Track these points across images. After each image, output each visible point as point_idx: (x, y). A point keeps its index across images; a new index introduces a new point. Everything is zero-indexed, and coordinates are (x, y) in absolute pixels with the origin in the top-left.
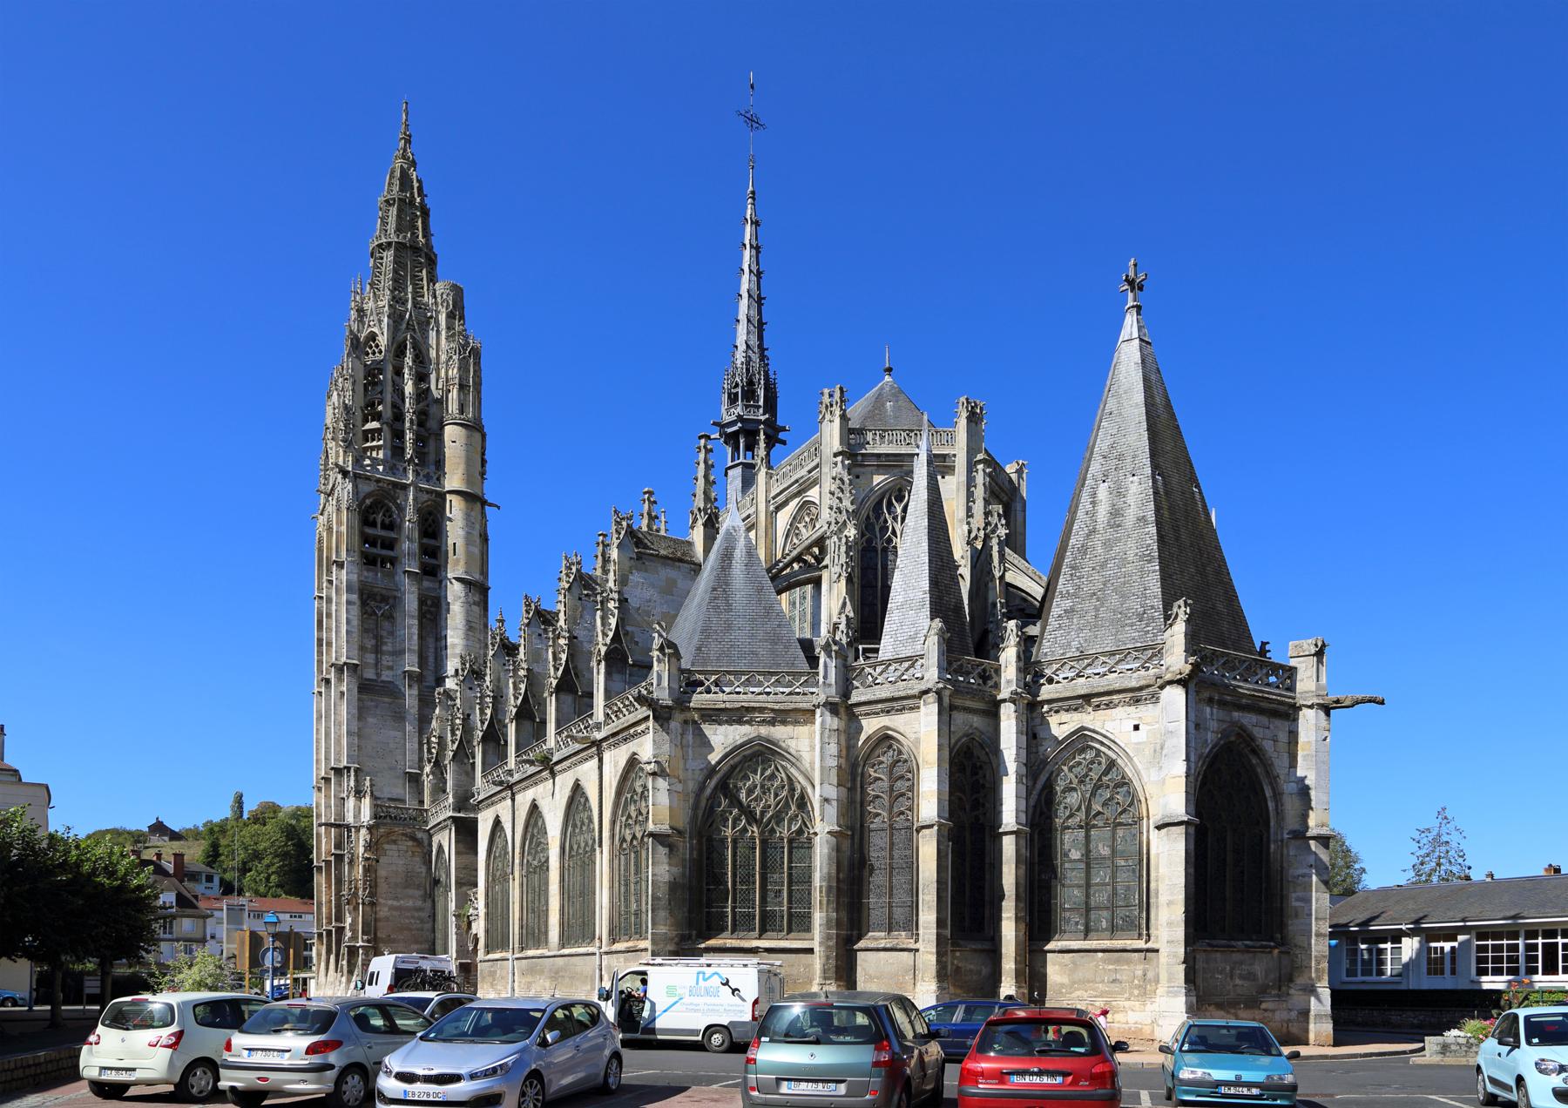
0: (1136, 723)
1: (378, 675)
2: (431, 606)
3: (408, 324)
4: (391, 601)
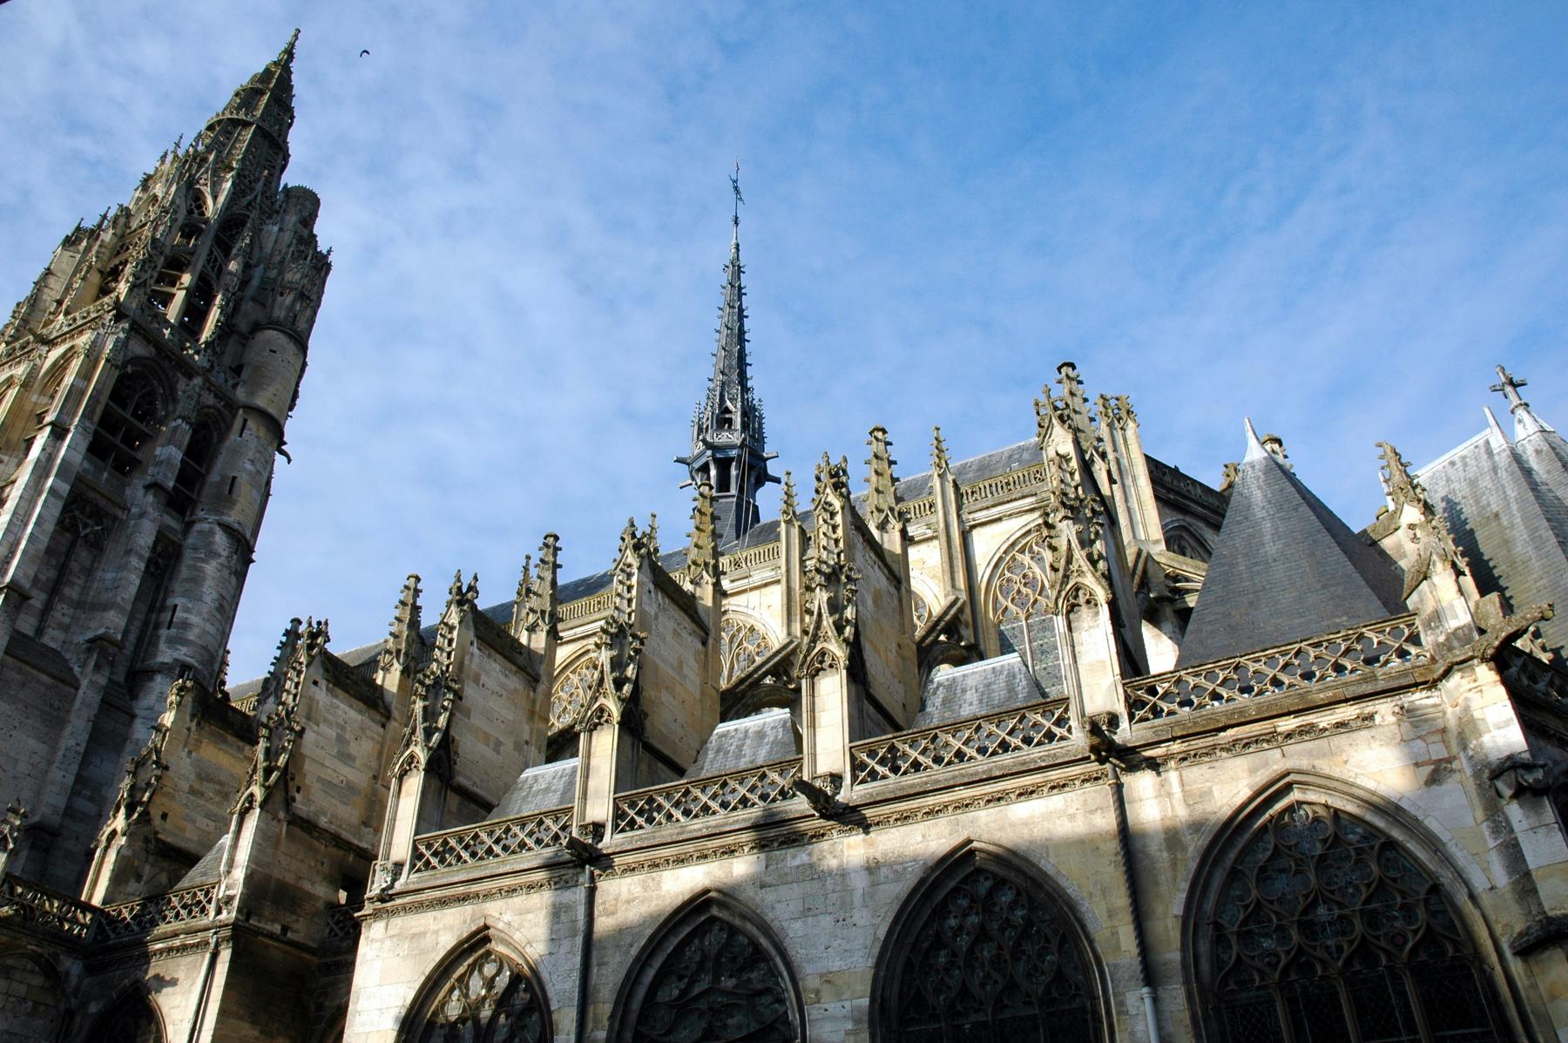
1: (40, 631)
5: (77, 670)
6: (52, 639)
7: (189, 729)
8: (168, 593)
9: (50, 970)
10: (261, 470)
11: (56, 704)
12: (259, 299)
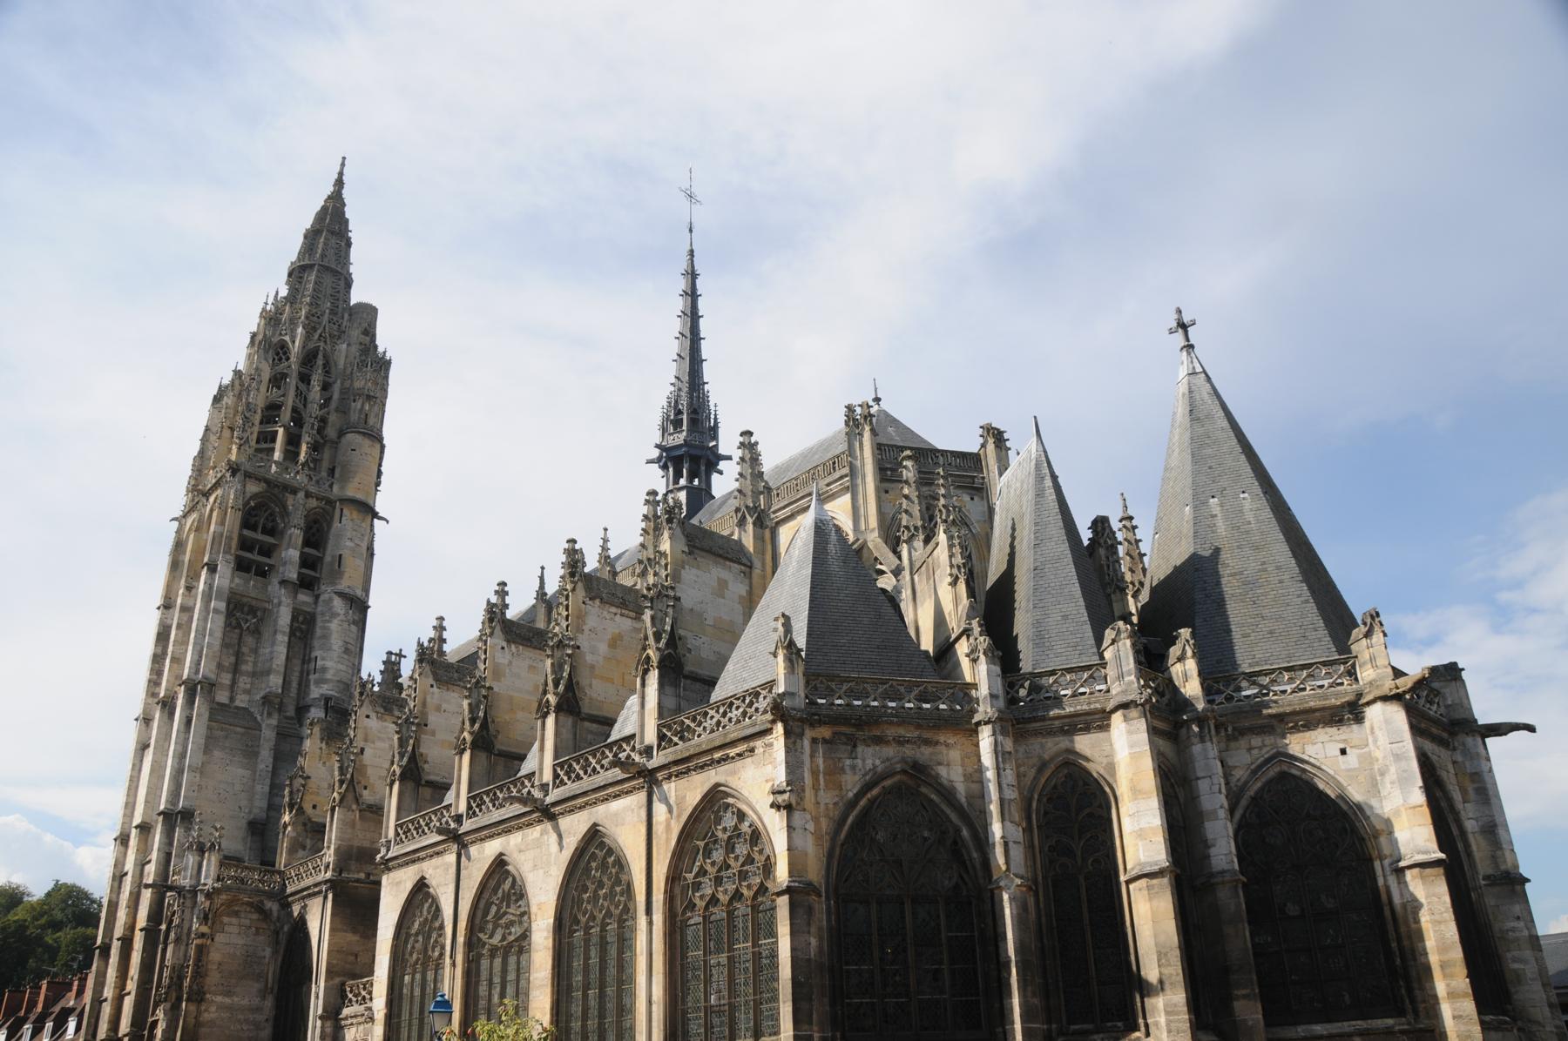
0: (1342, 746)
1: (232, 699)
2: (302, 623)
3: (320, 336)
4: (259, 614)
5: (259, 718)
6: (241, 701)
7: (321, 749)
8: (312, 648)
9: (260, 909)
10: (359, 543)
11: (250, 744)
12: (343, 410)
